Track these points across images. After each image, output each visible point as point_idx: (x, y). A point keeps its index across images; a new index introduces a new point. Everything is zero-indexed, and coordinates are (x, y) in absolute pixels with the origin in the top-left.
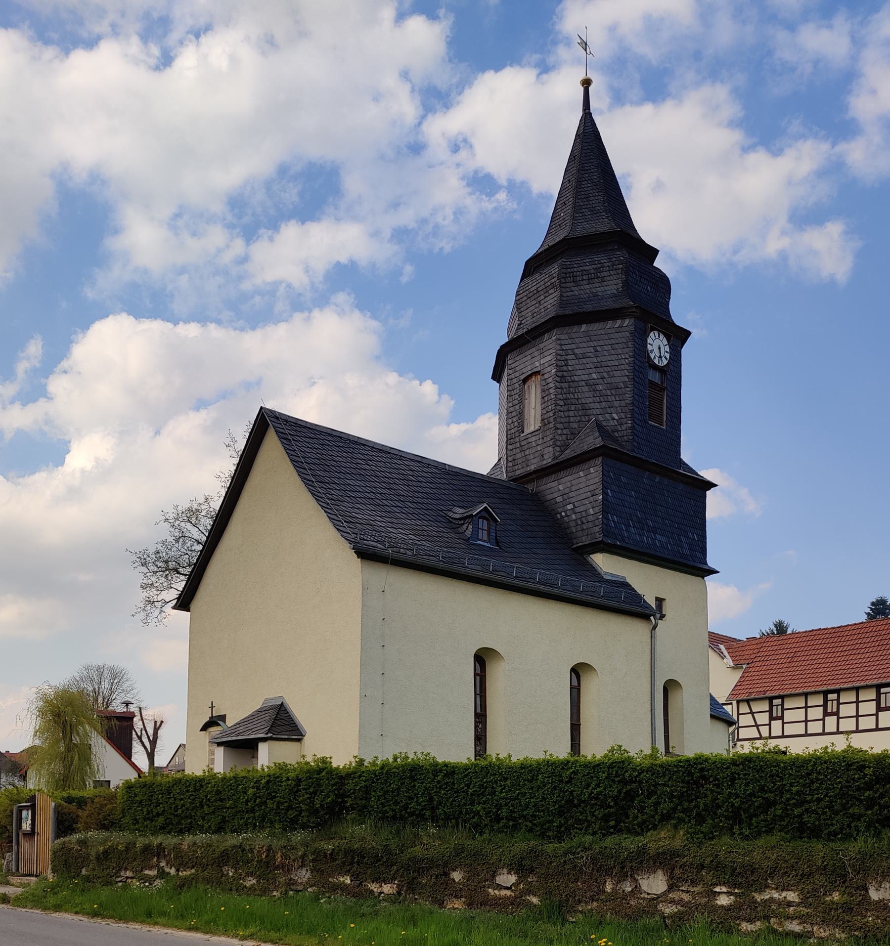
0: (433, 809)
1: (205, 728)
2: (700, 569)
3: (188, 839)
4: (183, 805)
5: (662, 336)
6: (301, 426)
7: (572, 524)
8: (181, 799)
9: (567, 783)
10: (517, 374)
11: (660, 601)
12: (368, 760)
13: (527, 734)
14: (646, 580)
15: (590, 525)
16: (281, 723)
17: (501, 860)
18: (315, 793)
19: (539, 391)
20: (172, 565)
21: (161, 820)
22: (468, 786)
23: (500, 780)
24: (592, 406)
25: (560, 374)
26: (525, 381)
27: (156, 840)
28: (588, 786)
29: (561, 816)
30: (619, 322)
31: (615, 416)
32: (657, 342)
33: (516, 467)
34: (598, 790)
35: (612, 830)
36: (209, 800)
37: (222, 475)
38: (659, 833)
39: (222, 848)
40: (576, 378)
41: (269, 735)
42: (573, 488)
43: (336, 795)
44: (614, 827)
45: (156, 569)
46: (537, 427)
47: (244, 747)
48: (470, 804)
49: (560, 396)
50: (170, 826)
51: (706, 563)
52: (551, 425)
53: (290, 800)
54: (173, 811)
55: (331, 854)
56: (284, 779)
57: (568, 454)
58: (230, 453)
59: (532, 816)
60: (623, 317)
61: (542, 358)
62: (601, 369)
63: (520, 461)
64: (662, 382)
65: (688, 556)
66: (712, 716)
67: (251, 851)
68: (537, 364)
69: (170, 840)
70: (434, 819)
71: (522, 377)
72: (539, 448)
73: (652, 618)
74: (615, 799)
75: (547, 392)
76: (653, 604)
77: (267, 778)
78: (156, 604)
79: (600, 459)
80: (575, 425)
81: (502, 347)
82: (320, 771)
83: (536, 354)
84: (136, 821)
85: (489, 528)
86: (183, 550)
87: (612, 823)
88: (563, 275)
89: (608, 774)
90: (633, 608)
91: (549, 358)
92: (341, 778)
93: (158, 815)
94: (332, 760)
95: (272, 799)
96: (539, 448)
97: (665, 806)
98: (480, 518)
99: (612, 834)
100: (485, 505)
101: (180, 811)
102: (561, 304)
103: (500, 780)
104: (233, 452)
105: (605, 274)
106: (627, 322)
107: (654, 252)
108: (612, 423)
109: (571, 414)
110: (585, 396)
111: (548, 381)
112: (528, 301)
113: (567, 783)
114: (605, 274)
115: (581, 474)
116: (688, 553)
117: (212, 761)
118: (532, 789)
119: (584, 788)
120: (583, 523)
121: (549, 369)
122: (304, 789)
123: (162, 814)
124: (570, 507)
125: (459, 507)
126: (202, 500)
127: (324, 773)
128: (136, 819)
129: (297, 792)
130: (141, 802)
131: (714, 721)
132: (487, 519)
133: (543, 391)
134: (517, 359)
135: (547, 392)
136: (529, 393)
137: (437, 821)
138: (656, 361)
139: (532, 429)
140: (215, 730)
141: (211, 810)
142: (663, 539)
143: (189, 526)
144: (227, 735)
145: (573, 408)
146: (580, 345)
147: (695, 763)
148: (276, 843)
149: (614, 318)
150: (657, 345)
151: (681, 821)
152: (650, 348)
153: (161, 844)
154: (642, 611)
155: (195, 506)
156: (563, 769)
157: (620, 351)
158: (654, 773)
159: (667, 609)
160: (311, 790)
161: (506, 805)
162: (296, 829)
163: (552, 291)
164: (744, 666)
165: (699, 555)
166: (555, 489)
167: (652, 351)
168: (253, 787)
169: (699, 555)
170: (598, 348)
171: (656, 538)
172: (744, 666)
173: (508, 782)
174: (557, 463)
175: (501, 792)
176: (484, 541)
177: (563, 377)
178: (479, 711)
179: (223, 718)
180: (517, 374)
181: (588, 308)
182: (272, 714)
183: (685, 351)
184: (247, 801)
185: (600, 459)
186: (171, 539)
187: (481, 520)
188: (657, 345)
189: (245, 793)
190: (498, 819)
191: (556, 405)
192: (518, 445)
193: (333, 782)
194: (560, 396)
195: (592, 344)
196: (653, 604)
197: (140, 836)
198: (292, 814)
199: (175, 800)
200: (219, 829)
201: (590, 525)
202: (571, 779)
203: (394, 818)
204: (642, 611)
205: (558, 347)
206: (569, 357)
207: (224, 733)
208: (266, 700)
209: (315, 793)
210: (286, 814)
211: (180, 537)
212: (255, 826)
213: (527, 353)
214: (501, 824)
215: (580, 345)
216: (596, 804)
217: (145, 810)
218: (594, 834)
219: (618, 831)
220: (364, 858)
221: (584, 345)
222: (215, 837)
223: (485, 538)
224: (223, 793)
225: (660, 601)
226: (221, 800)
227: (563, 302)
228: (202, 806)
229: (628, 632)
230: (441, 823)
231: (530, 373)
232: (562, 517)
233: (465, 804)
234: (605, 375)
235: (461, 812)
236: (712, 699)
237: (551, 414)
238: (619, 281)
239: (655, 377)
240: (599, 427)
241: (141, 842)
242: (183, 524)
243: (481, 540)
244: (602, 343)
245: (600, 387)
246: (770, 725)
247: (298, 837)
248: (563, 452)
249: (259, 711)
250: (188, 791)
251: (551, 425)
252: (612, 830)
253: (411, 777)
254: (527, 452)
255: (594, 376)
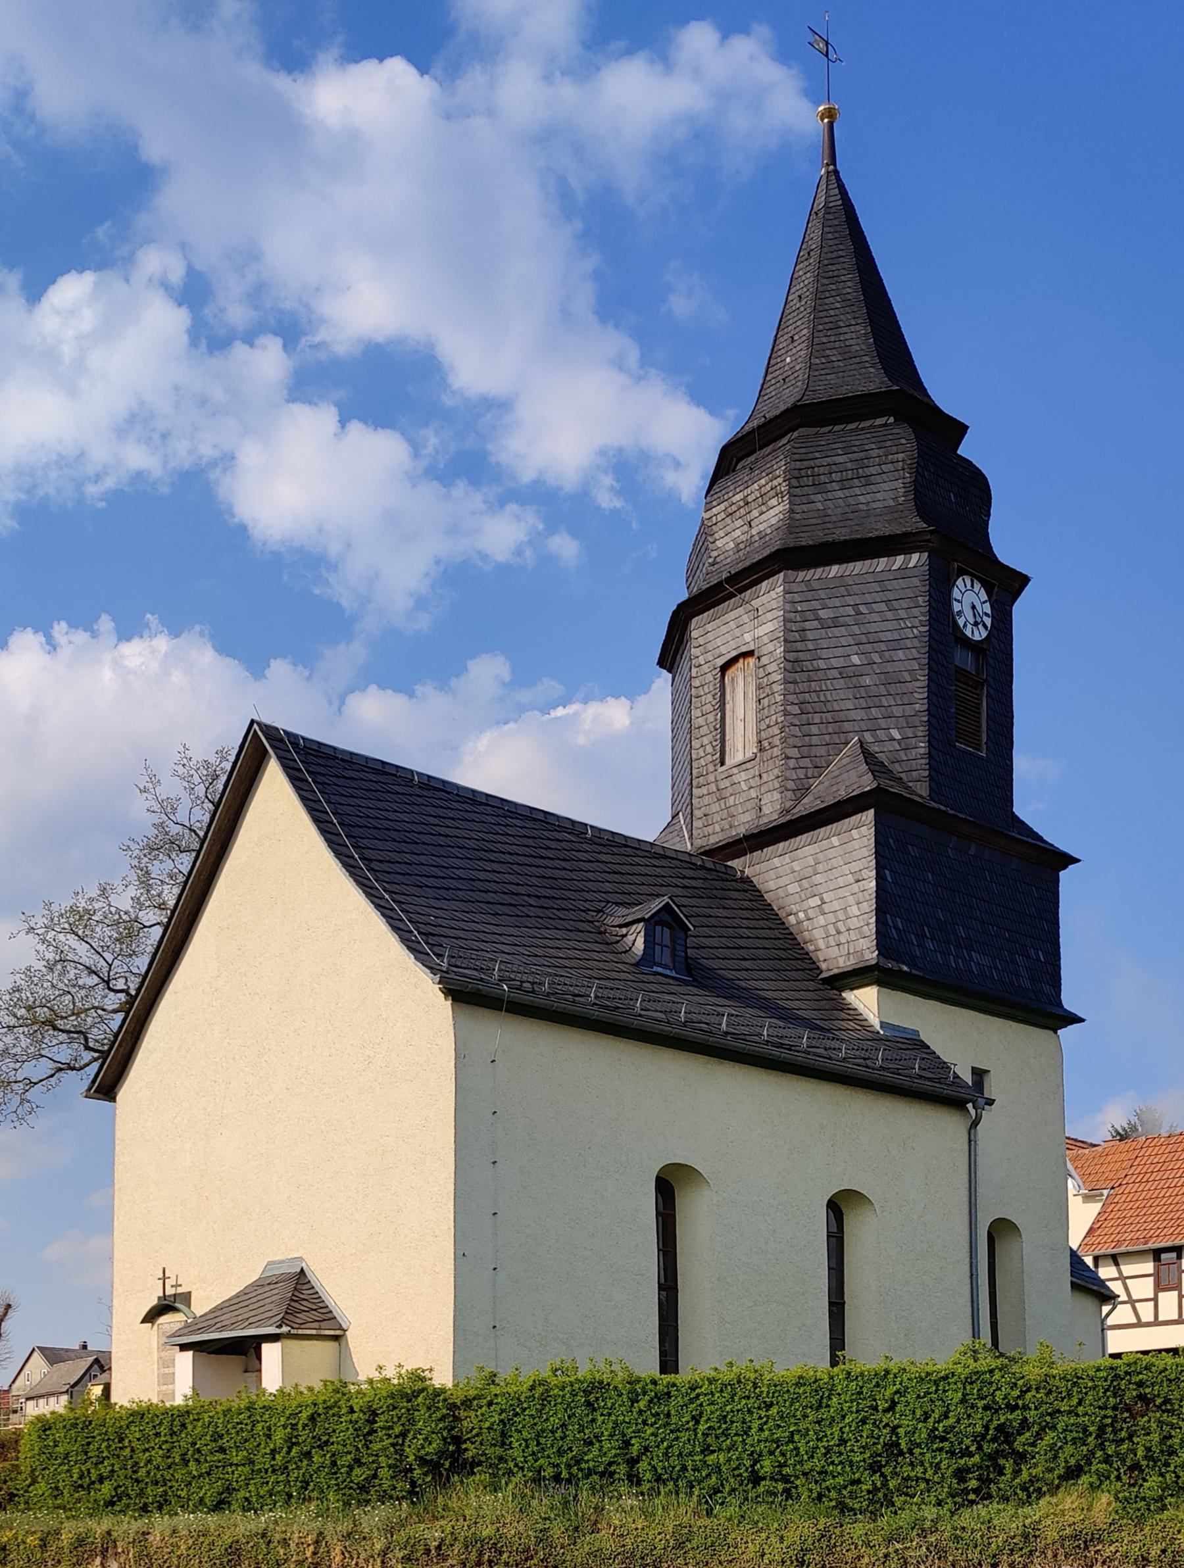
0: (633, 1462)
1: (152, 1316)
2: (1052, 1016)
3: (160, 1525)
4: (149, 1461)
5: (977, 586)
6: (327, 756)
7: (818, 934)
8: (147, 1450)
9: (886, 1411)
10: (709, 656)
11: (979, 1074)
12: (505, 1373)
13: (753, 1324)
14: (957, 1037)
15: (853, 935)
16: (298, 1305)
17: (763, 1555)
18: (404, 1435)
19: (752, 688)
20: (42, 1013)
21: (106, 1489)
22: (696, 1420)
23: (759, 1408)
24: (853, 715)
25: (791, 656)
26: (724, 668)
27: (100, 1526)
28: (926, 1416)
29: (875, 1472)
30: (900, 559)
31: (896, 734)
32: (969, 598)
33: (710, 829)
34: (946, 1423)
35: (972, 1497)
36: (199, 1451)
37: (133, 846)
38: (1063, 1501)
39: (227, 1539)
40: (822, 664)
41: (285, 1329)
42: (820, 868)
43: (444, 1439)
44: (976, 1491)
45: (13, 1021)
46: (749, 755)
47: (233, 1351)
48: (702, 1452)
49: (792, 698)
50: (125, 1500)
51: (1059, 1004)
52: (776, 752)
53: (358, 1449)
54: (129, 1472)
55: (439, 1548)
56: (344, 1411)
57: (810, 804)
58: (148, 804)
59: (819, 1473)
60: (908, 551)
61: (757, 623)
62: (868, 648)
63: (717, 818)
64: (978, 672)
65: (1032, 996)
66: (1074, 1286)
67: (285, 1542)
68: (748, 637)
69: (127, 1526)
70: (634, 1479)
71: (720, 662)
72: (753, 793)
73: (970, 1106)
74: (979, 1439)
75: (767, 690)
76: (968, 1078)
77: (310, 1411)
78: (15, 1086)
79: (872, 812)
80: (822, 751)
81: (680, 606)
82: (410, 1396)
83: (745, 618)
84: (57, 1492)
85: (673, 942)
86: (61, 985)
87: (973, 1484)
88: (796, 473)
89: (964, 1395)
90: (938, 1088)
91: (770, 627)
92: (453, 1407)
93: (101, 1480)
94: (435, 1375)
95: (321, 1447)
96: (753, 793)
97: (1070, 1454)
98: (657, 924)
99: (972, 1502)
100: (666, 899)
101: (142, 1473)
102: (789, 526)
103: (759, 1408)
104: (153, 803)
105: (873, 470)
106: (915, 557)
107: (960, 429)
108: (888, 746)
109: (814, 729)
110: (843, 700)
111: (770, 669)
112: (728, 520)
113: (886, 1411)
114: (873, 470)
115: (835, 841)
116: (1028, 985)
117: (168, 1379)
118: (819, 1422)
119: (919, 1420)
120: (839, 933)
121: (770, 647)
122: (382, 1428)
123: (109, 1478)
124: (815, 901)
125: (617, 904)
126: (94, 892)
127: (420, 1399)
128: (57, 1488)
129: (370, 1433)
130: (67, 1455)
131: (1077, 1294)
132: (670, 927)
133: (759, 687)
134: (709, 627)
135: (767, 690)
136: (733, 691)
137: (639, 1483)
138: (968, 632)
139: (740, 757)
140: (170, 1321)
141: (204, 1468)
142: (986, 961)
143: (72, 941)
144: (200, 1330)
145: (817, 718)
146: (830, 603)
147: (1127, 1373)
148: (335, 1529)
149: (891, 552)
150: (969, 600)
151: (1103, 1477)
152: (956, 607)
153: (109, 1533)
154: (959, 1096)
155: (82, 904)
156: (877, 1385)
157: (902, 614)
158: (1050, 1392)
159: (992, 1088)
160: (398, 1430)
161: (771, 1453)
162: (368, 1502)
163: (774, 502)
164: (1105, 1192)
165: (1047, 988)
166: (778, 873)
167: (960, 613)
168: (285, 1427)
169: (1047, 988)
170: (862, 609)
171: (971, 960)
172: (1105, 1192)
173: (774, 1411)
174: (790, 821)
175: (761, 1430)
176: (665, 967)
177: (796, 665)
178: (662, 1281)
179: (187, 1298)
180: (709, 656)
181: (842, 534)
182: (286, 1290)
183: (1019, 609)
184: (273, 1452)
185: (872, 812)
186: (39, 965)
187: (658, 928)
188: (969, 600)
189: (269, 1437)
190: (756, 1479)
191: (786, 714)
192: (713, 788)
193: (439, 1415)
194: (792, 698)
195: (850, 600)
196: (968, 1078)
197: (68, 1518)
198: (359, 1474)
199: (133, 1450)
200: (219, 1506)
201: (853, 935)
202: (894, 1404)
203: (557, 1478)
204: (959, 1096)
205: (788, 606)
206: (807, 625)
207: (188, 1328)
208: (268, 1264)
209: (404, 1435)
210: (349, 1474)
211: (57, 962)
212: (290, 1496)
213: (728, 617)
214: (761, 1489)
215: (830, 603)
216: (941, 1450)
217: (75, 1471)
218: (939, 1503)
219: (983, 1499)
220: (501, 1553)
221: (837, 602)
222: (212, 1520)
223: (667, 959)
224: (226, 1438)
225: (979, 1074)
226: (222, 1450)
227: (792, 523)
228: (186, 1463)
229: (932, 1132)
230: (645, 1487)
231: (734, 654)
232: (799, 922)
233: (690, 1454)
234: (876, 658)
235: (684, 1468)
236: (1071, 1249)
237: (776, 730)
238: (899, 483)
239: (964, 660)
240: (868, 756)
241: (69, 1532)
242: (61, 937)
243: (659, 965)
244: (868, 598)
245: (867, 681)
246: (1155, 1300)
247: (374, 1517)
248: (799, 800)
249: (257, 1285)
250: (157, 1435)
251: (776, 752)
252: (972, 1497)
253: (589, 1404)
254: (731, 801)
255: (856, 660)
